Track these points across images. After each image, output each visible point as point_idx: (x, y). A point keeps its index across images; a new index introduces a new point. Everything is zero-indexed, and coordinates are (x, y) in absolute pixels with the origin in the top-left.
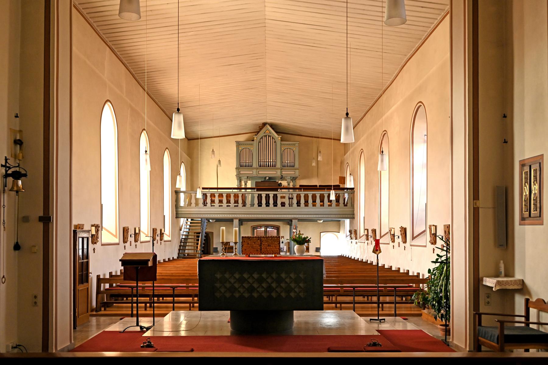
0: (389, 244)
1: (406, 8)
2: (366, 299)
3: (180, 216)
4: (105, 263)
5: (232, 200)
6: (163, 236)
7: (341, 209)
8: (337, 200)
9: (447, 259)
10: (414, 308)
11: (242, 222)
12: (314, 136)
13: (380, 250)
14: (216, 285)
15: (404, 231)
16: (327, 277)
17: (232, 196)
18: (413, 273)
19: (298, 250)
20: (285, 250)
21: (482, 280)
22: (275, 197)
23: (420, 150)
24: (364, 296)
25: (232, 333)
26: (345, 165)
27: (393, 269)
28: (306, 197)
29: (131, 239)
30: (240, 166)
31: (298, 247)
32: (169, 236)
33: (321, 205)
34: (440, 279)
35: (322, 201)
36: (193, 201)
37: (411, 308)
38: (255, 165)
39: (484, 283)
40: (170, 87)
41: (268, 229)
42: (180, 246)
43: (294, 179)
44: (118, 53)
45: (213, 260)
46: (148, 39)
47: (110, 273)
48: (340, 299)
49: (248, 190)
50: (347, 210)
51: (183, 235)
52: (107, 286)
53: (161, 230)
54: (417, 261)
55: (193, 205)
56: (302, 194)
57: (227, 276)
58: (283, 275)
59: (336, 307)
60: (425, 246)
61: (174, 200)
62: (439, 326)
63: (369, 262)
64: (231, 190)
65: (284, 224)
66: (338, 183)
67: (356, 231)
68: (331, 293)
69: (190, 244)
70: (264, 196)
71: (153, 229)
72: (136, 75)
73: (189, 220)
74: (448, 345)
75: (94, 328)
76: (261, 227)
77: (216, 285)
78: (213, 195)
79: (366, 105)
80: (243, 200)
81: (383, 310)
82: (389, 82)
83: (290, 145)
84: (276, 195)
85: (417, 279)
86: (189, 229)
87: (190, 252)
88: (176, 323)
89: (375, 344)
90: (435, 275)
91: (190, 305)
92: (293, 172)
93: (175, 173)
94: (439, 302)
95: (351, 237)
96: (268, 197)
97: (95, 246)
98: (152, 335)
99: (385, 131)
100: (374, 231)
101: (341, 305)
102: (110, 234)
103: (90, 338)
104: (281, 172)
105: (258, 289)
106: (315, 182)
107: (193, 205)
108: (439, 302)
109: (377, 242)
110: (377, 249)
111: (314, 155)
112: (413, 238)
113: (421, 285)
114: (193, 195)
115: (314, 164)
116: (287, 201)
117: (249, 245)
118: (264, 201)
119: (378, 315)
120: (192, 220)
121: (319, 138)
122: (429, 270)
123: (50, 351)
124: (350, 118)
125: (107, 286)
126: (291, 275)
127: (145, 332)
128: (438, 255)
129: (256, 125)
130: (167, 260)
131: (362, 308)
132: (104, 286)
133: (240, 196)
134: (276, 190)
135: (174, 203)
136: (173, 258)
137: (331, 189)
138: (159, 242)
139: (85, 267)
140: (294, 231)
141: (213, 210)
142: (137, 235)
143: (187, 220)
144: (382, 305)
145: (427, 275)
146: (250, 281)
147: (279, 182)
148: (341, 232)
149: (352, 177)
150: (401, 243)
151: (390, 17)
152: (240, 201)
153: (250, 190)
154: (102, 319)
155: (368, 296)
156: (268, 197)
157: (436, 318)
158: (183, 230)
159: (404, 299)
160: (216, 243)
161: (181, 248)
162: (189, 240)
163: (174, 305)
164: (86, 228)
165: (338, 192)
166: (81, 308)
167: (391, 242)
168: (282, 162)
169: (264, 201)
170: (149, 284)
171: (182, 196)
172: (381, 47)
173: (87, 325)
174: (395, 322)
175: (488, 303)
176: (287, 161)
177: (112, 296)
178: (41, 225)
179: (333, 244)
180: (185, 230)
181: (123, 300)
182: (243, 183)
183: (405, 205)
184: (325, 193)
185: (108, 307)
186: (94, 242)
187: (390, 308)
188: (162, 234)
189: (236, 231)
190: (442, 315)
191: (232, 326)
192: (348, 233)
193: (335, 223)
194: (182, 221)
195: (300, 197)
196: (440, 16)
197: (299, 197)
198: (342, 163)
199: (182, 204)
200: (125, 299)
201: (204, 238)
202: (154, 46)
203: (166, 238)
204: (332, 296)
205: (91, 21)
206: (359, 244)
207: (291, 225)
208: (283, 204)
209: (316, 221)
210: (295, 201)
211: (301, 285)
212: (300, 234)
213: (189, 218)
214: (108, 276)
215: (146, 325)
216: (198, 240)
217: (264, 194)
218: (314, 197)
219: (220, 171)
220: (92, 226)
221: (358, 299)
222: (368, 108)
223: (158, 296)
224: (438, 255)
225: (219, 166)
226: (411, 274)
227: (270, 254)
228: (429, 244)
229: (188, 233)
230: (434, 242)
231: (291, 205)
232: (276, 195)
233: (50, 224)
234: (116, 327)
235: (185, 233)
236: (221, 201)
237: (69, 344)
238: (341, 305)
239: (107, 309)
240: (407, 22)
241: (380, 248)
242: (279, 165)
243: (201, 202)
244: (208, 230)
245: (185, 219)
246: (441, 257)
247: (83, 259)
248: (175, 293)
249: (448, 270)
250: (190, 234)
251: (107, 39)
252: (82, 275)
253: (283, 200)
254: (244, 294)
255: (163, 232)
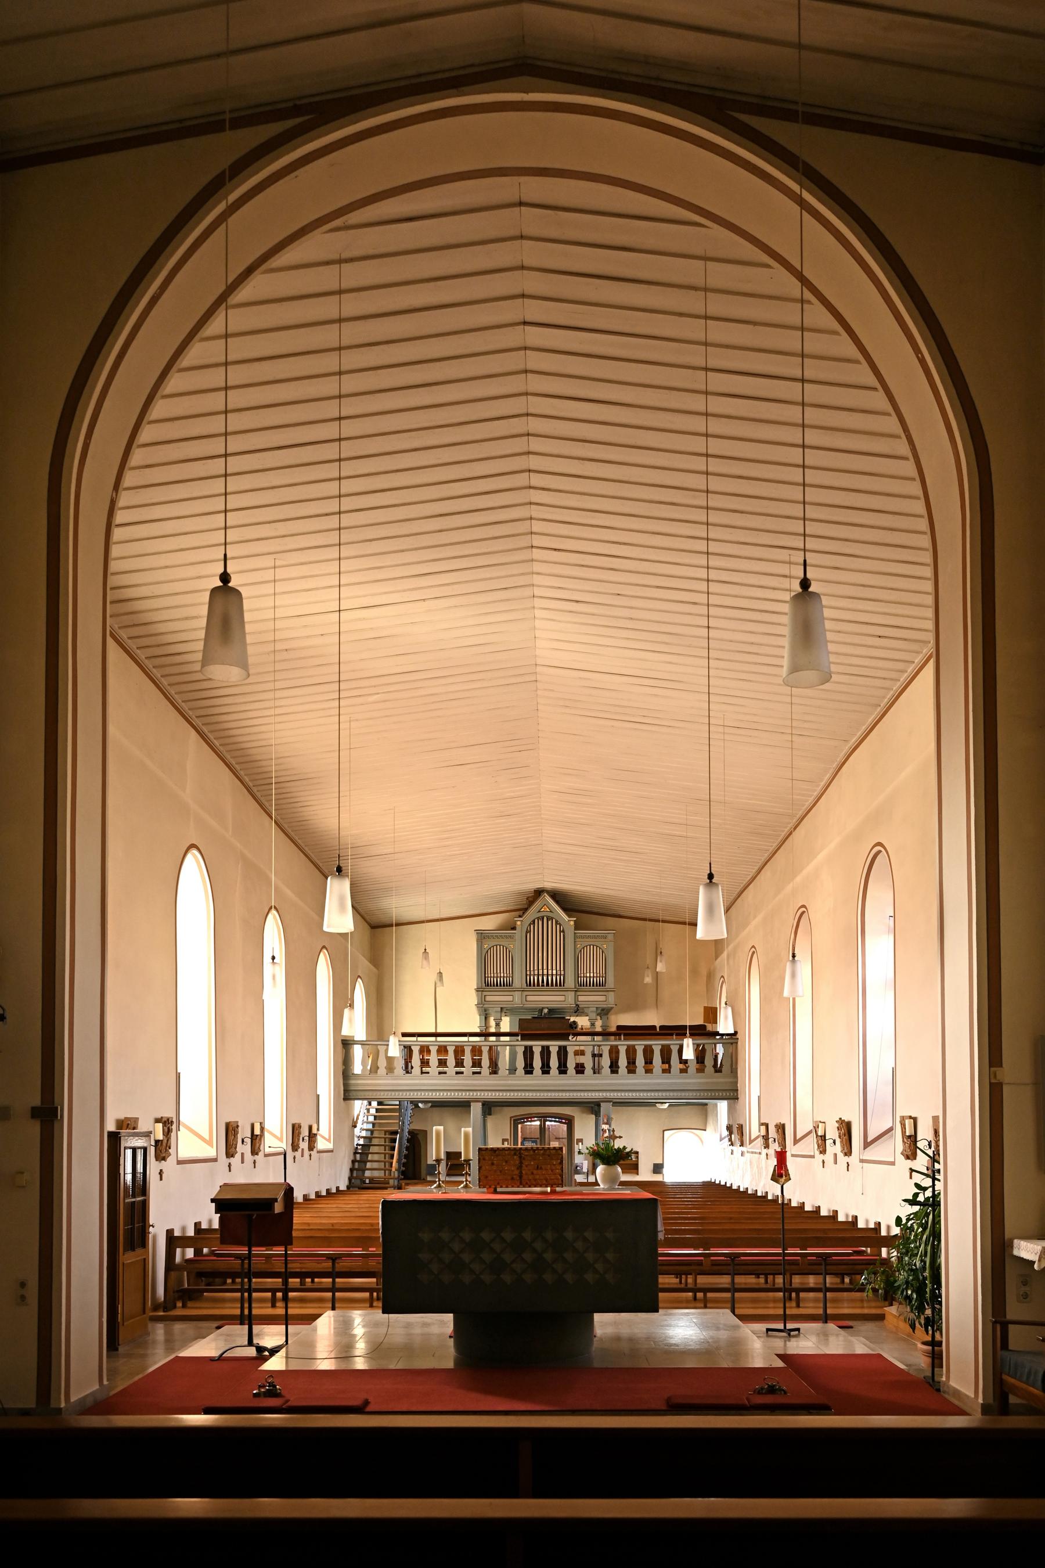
0: (813, 1157)
1: (831, 647)
2: (762, 1280)
3: (352, 1094)
4: (182, 1205)
5: (468, 1059)
6: (315, 1141)
7: (708, 1079)
8: (700, 1056)
9: (935, 1196)
10: (869, 1301)
11: (489, 1107)
12: (648, 917)
13: (787, 1175)
14: (420, 1255)
15: (846, 1128)
16: (667, 1232)
17: (468, 1051)
18: (867, 1222)
19: (604, 1176)
20: (585, 1170)
21: (1012, 1247)
22: (563, 1053)
23: (879, 949)
24: (758, 1276)
25: (457, 1362)
26: (718, 982)
27: (824, 1213)
28: (631, 1053)
29: (244, 1149)
30: (486, 985)
31: (605, 1170)
32: (329, 1140)
33: (664, 1071)
34: (921, 1238)
35: (666, 1058)
36: (382, 1063)
37: (862, 1301)
38: (518, 982)
39: (1016, 1253)
40: (328, 814)
41: (548, 1123)
42: (353, 1162)
43: (604, 1012)
44: (217, 743)
45: (415, 1201)
46: (278, 711)
47: (197, 1225)
48: (703, 1280)
49: (502, 1038)
50: (720, 1080)
51: (359, 1137)
52: (190, 1253)
53: (310, 1128)
54: (871, 1195)
55: (382, 1071)
56: (623, 1045)
57: (445, 1235)
58: (569, 1235)
59: (695, 1298)
60: (893, 1163)
61: (340, 1060)
62: (920, 1346)
63: (770, 1197)
64: (465, 1039)
65: (583, 1112)
66: (701, 1022)
67: (741, 1128)
68: (681, 1267)
69: (376, 1157)
70: (537, 1051)
71: (294, 1126)
72: (255, 789)
73: (374, 1104)
74: (938, 1390)
75: (160, 1350)
76: (530, 1117)
77: (420, 1255)
78: (425, 1050)
79: (778, 836)
80: (491, 1059)
81: (798, 1306)
82: (811, 800)
83: (595, 937)
84: (565, 1047)
85: (873, 1236)
86: (374, 1125)
87: (376, 1174)
88: (338, 1338)
89: (772, 1390)
90: (911, 1228)
91: (371, 1295)
92: (603, 998)
93: (342, 1001)
94: (920, 1290)
95: (730, 1140)
96: (546, 1052)
97: (163, 1165)
98: (284, 1368)
99: (803, 906)
100: (781, 1128)
101: (705, 1295)
102: (195, 1140)
103: (151, 1369)
104: (576, 997)
105: (514, 1265)
106: (651, 1018)
107: (382, 1071)
108: (920, 1290)
109: (781, 1157)
110: (780, 1173)
111: (649, 960)
112: (867, 1144)
113: (884, 1250)
114: (382, 1049)
115: (648, 980)
116: (587, 1061)
117: (494, 1168)
118: (537, 1063)
119: (785, 1318)
120: (379, 1104)
121: (658, 921)
122: (898, 1220)
123: (53, 1405)
124: (716, 885)
125: (190, 1253)
126: (586, 1234)
127: (265, 1359)
128: (917, 1186)
129: (520, 893)
130: (324, 1193)
131: (754, 1301)
132: (183, 1254)
133: (485, 1050)
134: (564, 1037)
135: (341, 1068)
136: (337, 1188)
137: (685, 1035)
138: (307, 1153)
139: (140, 1213)
140: (605, 1127)
141: (425, 1081)
142: (256, 1140)
143: (370, 1104)
144: (798, 1296)
145: (896, 1231)
146: (497, 1246)
147: (572, 1019)
148: (710, 1128)
149: (730, 1009)
150: (840, 1155)
151: (795, 669)
152: (485, 1062)
153: (507, 1038)
154: (178, 1327)
155: (766, 1275)
156: (546, 1052)
157: (913, 1327)
158: (359, 1125)
159: (847, 1280)
160: (435, 1151)
161: (356, 1165)
162: (373, 1149)
163: (334, 1295)
164: (143, 1127)
165: (701, 1041)
166: (128, 1304)
167: (817, 1153)
168: (577, 976)
169: (537, 1063)
170: (279, 1250)
171: (358, 1051)
172: (789, 723)
173: (142, 1341)
174: (825, 1335)
175: (1026, 1296)
176: (591, 972)
177: (200, 1275)
178: (35, 1129)
179: (692, 1155)
180: (365, 1126)
181: (225, 1283)
182: (492, 1023)
183: (841, 1074)
184: (673, 1043)
185: (191, 1299)
186: (161, 1157)
187: (816, 1300)
188: (312, 1137)
189: (466, 1135)
190: (927, 1319)
191: (458, 1346)
192: (726, 1133)
193: (695, 1107)
194: (359, 1107)
195: (618, 1052)
196: (921, 656)
197: (614, 1052)
198: (710, 976)
199: (357, 1068)
200: (229, 1281)
201: (405, 1143)
202: (289, 728)
203: (321, 1144)
204: (686, 1274)
205: (157, 673)
206: (747, 1155)
207: (597, 1114)
208: (580, 1069)
209: (653, 1104)
210: (606, 1061)
211: (610, 1256)
212: (613, 1137)
213: (374, 1099)
214: (191, 1232)
215: (269, 1342)
216: (393, 1149)
217: (537, 1046)
218: (648, 1052)
219: (443, 995)
220: (157, 1121)
221: (741, 1280)
222: (766, 855)
223: (302, 1275)
224: (917, 1186)
225: (438, 984)
226: (861, 1225)
227: (541, 1186)
228: (900, 1159)
229: (372, 1132)
230: (911, 1155)
231: (596, 1071)
232: (565, 1047)
233: (56, 1125)
234: (206, 1347)
235: (364, 1134)
236: (442, 1063)
237: (97, 1387)
238: (705, 1295)
239: (189, 1304)
240: (834, 677)
241: (787, 1170)
242: (570, 982)
243: (400, 1064)
244: (414, 1127)
245: (365, 1102)
246: (925, 1189)
247: (134, 1196)
248: (337, 1270)
249: (936, 1222)
250: (376, 1134)
251: (191, 713)
252: (132, 1229)
253: (581, 1059)
254: (482, 1277)
255: (314, 1131)
